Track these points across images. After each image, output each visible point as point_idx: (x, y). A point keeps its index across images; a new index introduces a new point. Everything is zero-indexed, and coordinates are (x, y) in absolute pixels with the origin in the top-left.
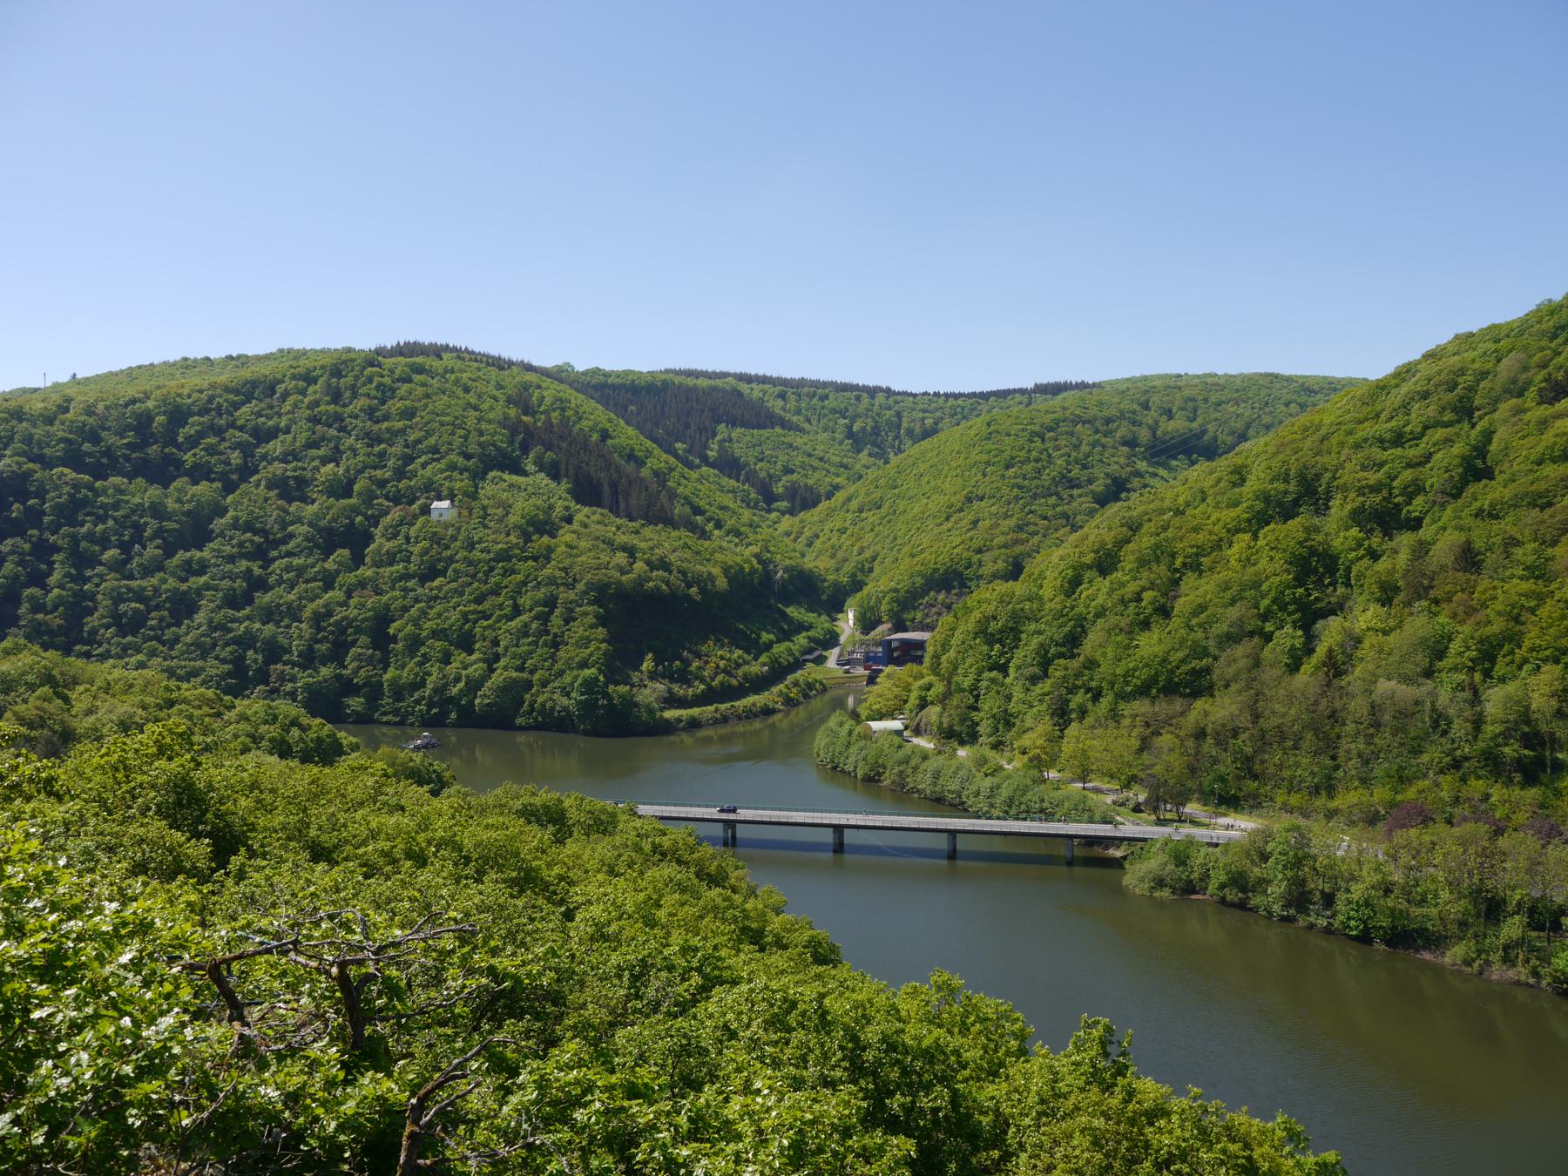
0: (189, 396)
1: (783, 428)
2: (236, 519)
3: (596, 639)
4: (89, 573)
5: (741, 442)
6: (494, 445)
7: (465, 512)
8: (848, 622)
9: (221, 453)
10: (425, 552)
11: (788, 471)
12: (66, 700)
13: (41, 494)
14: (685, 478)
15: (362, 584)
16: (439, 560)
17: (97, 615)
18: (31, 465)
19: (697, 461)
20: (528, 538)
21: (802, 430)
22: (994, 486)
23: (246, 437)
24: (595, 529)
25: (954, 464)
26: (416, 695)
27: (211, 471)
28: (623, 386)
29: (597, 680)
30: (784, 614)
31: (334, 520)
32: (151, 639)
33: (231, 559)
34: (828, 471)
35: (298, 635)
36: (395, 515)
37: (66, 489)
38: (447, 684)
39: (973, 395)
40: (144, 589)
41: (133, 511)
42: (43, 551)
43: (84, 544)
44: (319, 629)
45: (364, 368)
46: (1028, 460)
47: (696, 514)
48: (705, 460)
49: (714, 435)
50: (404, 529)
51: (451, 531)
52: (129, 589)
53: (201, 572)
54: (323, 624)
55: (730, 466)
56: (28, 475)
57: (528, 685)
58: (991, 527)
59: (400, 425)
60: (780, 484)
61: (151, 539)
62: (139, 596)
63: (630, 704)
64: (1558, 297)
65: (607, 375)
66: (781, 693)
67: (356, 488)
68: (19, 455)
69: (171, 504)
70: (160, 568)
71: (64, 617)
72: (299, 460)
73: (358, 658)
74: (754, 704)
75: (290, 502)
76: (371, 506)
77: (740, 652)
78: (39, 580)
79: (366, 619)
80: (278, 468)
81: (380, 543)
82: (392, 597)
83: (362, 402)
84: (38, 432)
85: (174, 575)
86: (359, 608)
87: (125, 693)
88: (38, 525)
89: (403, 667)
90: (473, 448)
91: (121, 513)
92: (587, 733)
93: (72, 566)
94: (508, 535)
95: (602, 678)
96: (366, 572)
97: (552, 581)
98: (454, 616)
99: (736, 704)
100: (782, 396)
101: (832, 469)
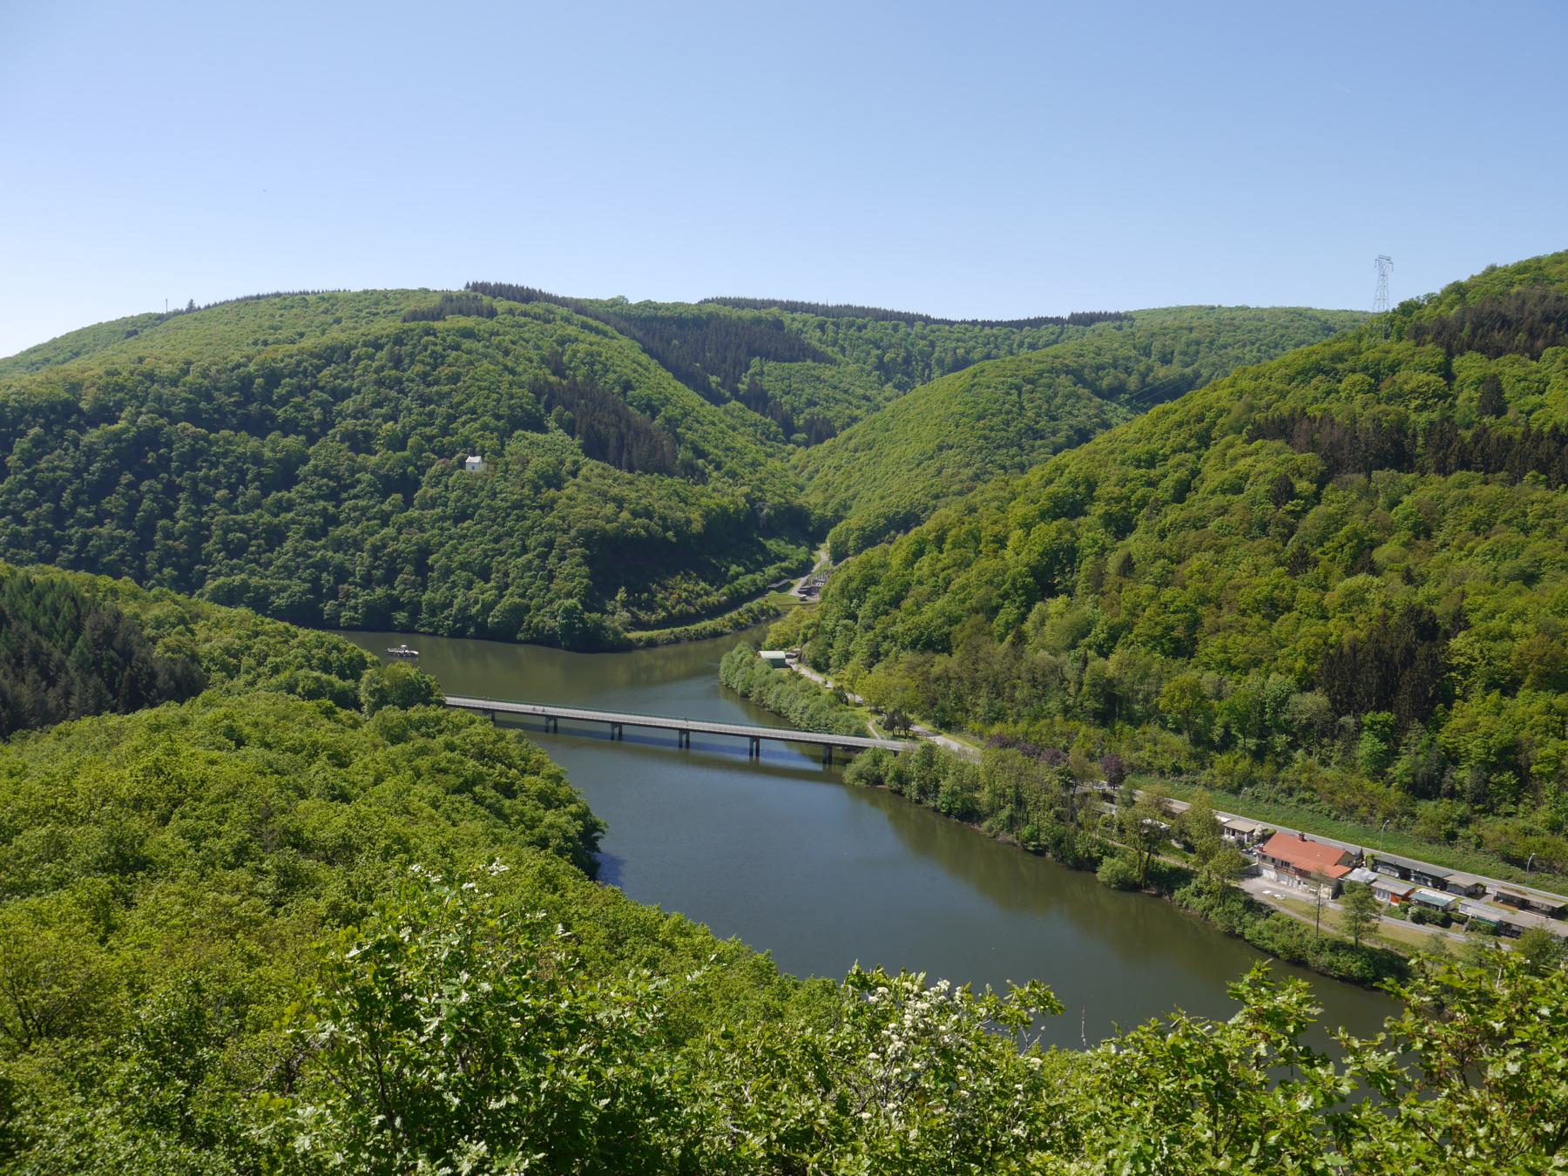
0: (282, 361)
1: (814, 361)
2: (316, 466)
3: (580, 576)
4: (205, 508)
5: (770, 374)
6: (521, 407)
7: (492, 467)
8: (823, 555)
9: (306, 410)
10: (459, 499)
11: (811, 403)
12: (192, 632)
13: (169, 445)
14: (698, 422)
15: (410, 523)
16: (469, 506)
17: (211, 541)
18: (161, 421)
19: (728, 394)
20: (537, 489)
21: (832, 361)
22: (963, 436)
23: (325, 396)
24: (596, 483)
25: (936, 414)
26: (446, 613)
27: (298, 425)
28: (671, 318)
29: (576, 608)
30: (762, 548)
31: (391, 469)
32: (251, 562)
33: (312, 499)
34: (850, 403)
35: (360, 563)
36: (437, 467)
37: (188, 441)
38: (468, 605)
39: (1011, 324)
40: (245, 522)
41: (238, 459)
42: (172, 490)
43: (201, 485)
44: (376, 558)
45: (421, 337)
46: (1000, 412)
47: (699, 458)
48: (736, 394)
49: (748, 368)
50: (444, 479)
51: (479, 483)
52: (236, 522)
53: (288, 510)
54: (380, 554)
55: (758, 400)
56: (159, 429)
57: (527, 609)
58: (953, 475)
59: (446, 389)
60: (802, 416)
61: (252, 481)
62: (242, 528)
63: (599, 627)
64: (1561, 250)
65: (657, 307)
66: (731, 620)
67: (410, 442)
68: (152, 412)
69: (268, 454)
70: (259, 506)
71: (188, 543)
72: (367, 417)
73: (404, 582)
74: (705, 628)
75: (358, 454)
76: (420, 458)
77: (702, 584)
78: (168, 513)
79: (411, 552)
80: (349, 424)
81: (426, 491)
82: (431, 534)
83: (418, 368)
84: (166, 392)
85: (268, 511)
86: (406, 544)
87: (229, 627)
88: (167, 469)
89: (438, 589)
90: (504, 411)
91: (229, 460)
92: (567, 649)
93: (193, 503)
94: (523, 487)
95: (580, 607)
96: (414, 513)
97: (551, 527)
98: (477, 552)
99: (689, 628)
100: (822, 326)
101: (855, 402)
